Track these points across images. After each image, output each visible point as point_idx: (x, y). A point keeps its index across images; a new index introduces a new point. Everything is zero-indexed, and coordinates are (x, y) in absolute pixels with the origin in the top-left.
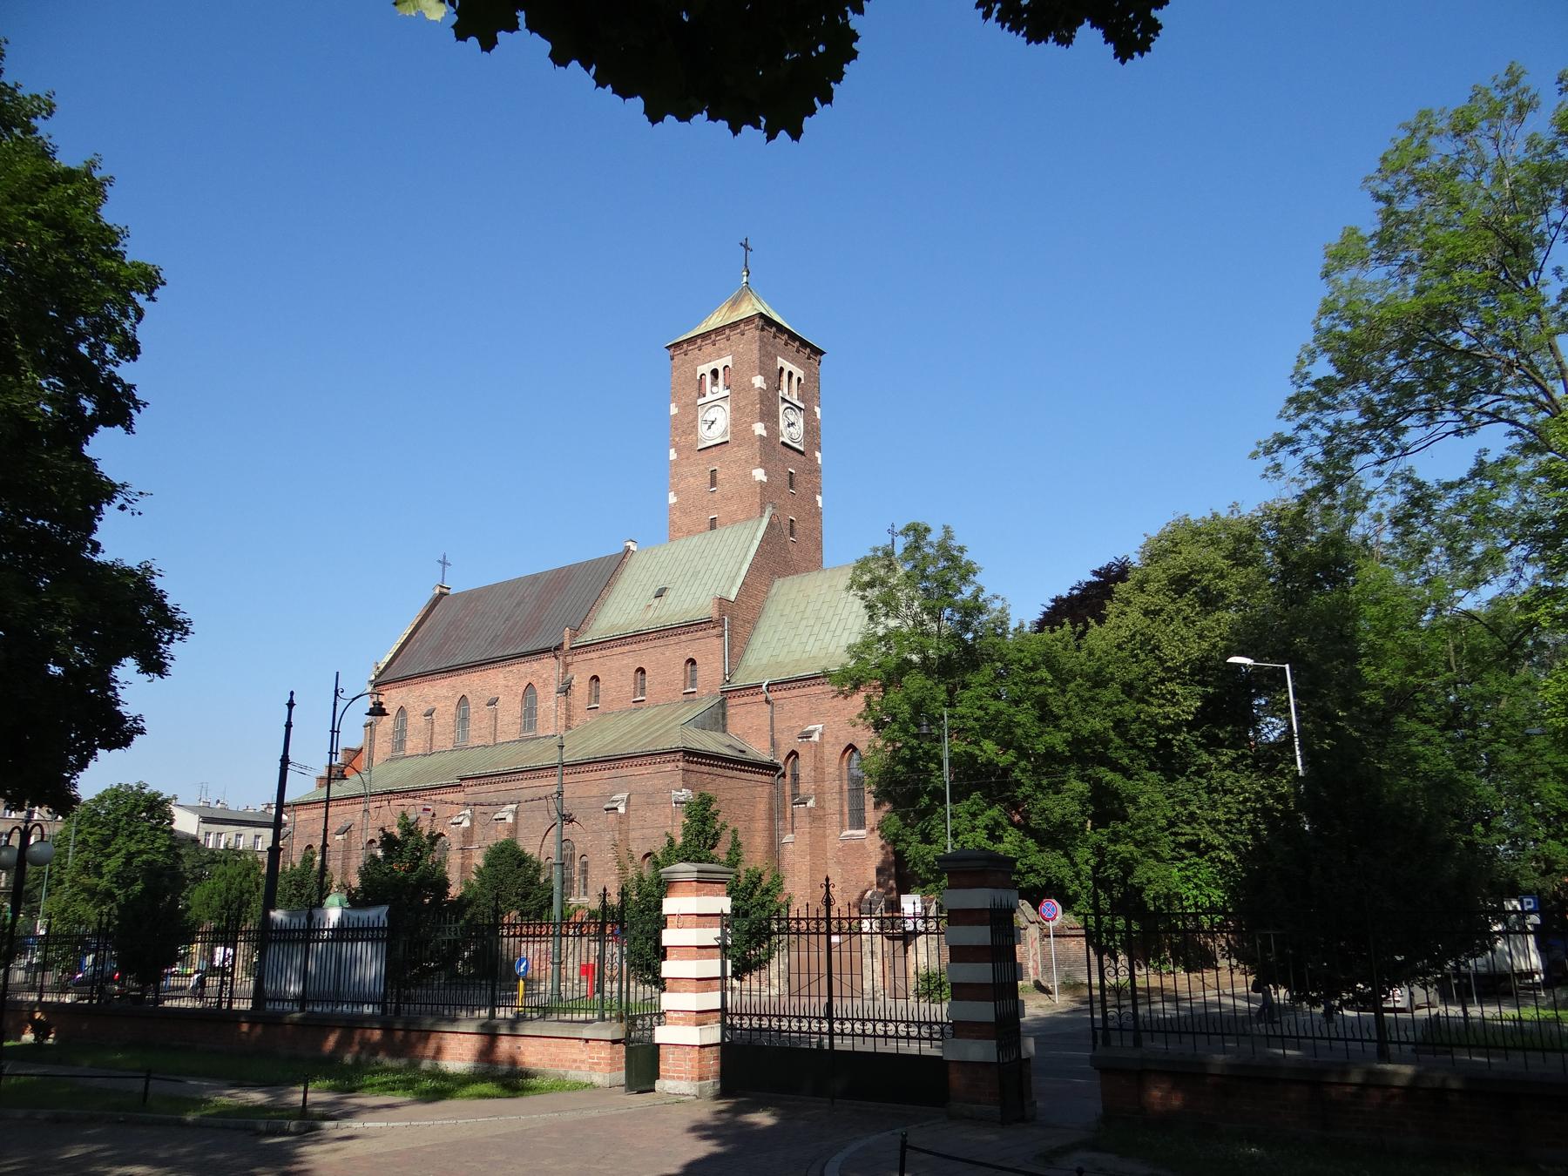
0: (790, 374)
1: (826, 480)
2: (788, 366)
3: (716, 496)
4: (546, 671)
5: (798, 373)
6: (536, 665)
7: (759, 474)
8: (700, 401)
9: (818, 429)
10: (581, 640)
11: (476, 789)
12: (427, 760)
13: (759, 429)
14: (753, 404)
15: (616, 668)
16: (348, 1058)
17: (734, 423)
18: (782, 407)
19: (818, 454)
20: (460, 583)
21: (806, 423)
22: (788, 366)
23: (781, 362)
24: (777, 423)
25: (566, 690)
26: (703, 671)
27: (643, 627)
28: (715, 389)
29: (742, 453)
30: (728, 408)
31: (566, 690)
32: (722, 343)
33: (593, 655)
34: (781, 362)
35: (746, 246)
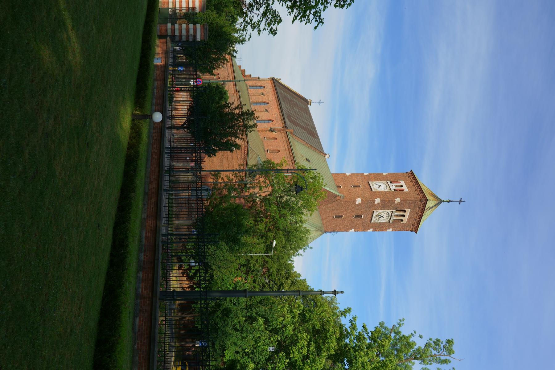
0: (404, 216)
1: (361, 233)
2: (407, 214)
3: (350, 188)
4: (278, 124)
5: (405, 219)
6: (280, 122)
7: (359, 201)
8: (389, 182)
9: (383, 230)
10: (289, 135)
11: (235, 96)
12: (246, 93)
13: (378, 201)
14: (388, 198)
15: (281, 144)
16: (169, 25)
17: (380, 193)
18: (389, 211)
19: (372, 230)
20: (312, 108)
21: (384, 223)
22: (407, 214)
23: (408, 211)
24: (381, 209)
25: (271, 130)
26: (274, 142)
27: (294, 151)
28: (394, 187)
29: (367, 195)
30: (386, 190)
31: (271, 130)
32: (411, 184)
33: (284, 138)
34: (408, 211)
35: (460, 201)
